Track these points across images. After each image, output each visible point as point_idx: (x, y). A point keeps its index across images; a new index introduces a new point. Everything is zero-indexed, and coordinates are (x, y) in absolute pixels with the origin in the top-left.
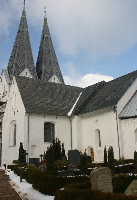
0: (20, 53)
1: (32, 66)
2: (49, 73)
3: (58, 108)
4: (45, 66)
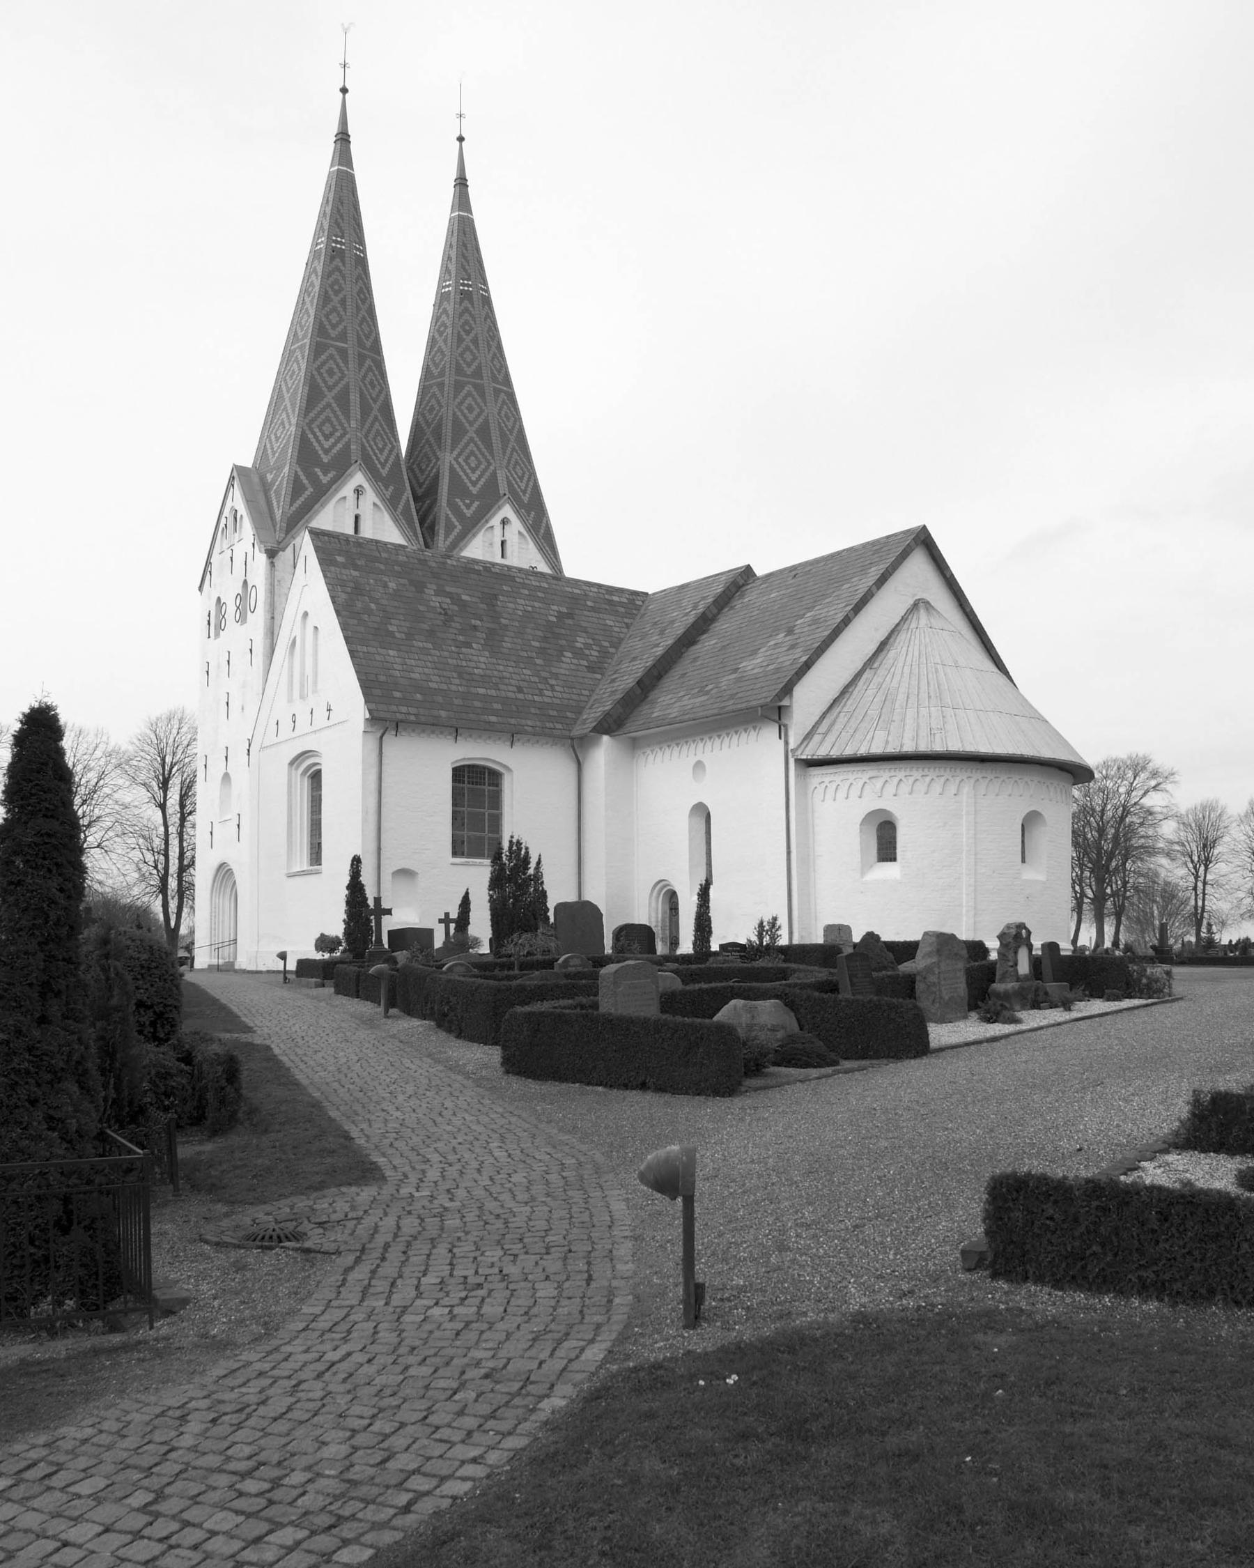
0: (325, 382)
1: (386, 451)
2: (474, 490)
3: (520, 696)
4: (455, 453)
